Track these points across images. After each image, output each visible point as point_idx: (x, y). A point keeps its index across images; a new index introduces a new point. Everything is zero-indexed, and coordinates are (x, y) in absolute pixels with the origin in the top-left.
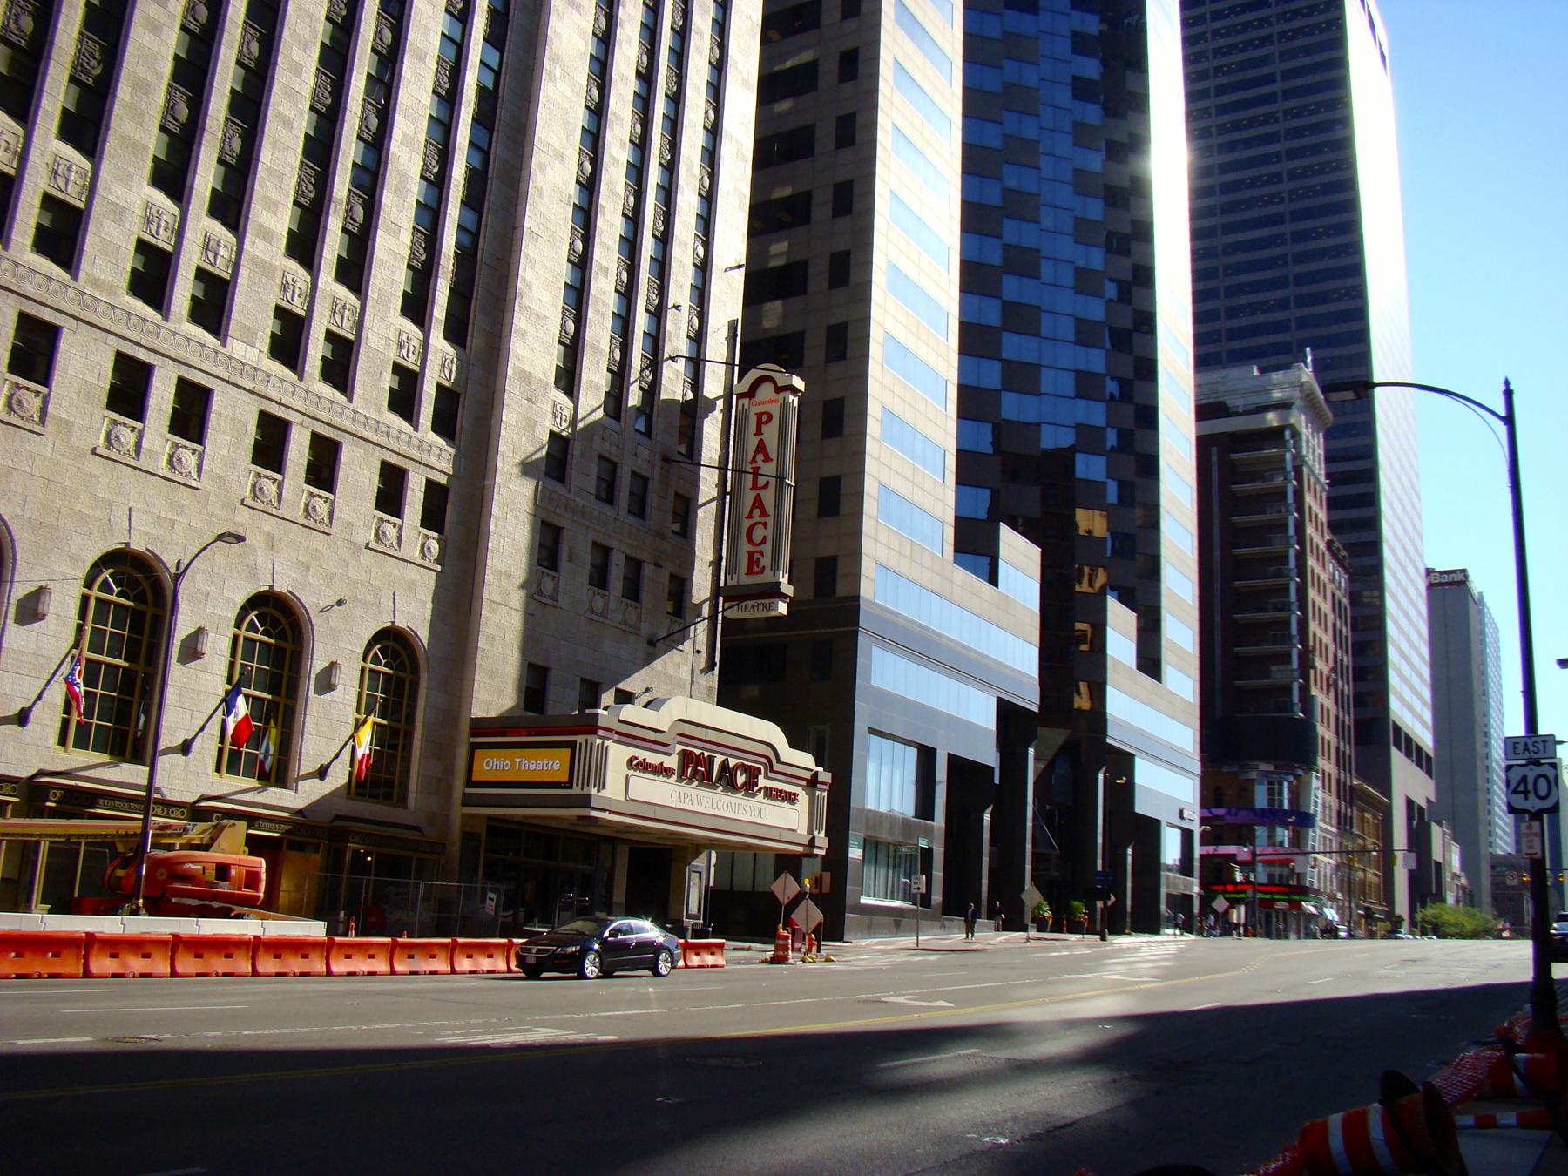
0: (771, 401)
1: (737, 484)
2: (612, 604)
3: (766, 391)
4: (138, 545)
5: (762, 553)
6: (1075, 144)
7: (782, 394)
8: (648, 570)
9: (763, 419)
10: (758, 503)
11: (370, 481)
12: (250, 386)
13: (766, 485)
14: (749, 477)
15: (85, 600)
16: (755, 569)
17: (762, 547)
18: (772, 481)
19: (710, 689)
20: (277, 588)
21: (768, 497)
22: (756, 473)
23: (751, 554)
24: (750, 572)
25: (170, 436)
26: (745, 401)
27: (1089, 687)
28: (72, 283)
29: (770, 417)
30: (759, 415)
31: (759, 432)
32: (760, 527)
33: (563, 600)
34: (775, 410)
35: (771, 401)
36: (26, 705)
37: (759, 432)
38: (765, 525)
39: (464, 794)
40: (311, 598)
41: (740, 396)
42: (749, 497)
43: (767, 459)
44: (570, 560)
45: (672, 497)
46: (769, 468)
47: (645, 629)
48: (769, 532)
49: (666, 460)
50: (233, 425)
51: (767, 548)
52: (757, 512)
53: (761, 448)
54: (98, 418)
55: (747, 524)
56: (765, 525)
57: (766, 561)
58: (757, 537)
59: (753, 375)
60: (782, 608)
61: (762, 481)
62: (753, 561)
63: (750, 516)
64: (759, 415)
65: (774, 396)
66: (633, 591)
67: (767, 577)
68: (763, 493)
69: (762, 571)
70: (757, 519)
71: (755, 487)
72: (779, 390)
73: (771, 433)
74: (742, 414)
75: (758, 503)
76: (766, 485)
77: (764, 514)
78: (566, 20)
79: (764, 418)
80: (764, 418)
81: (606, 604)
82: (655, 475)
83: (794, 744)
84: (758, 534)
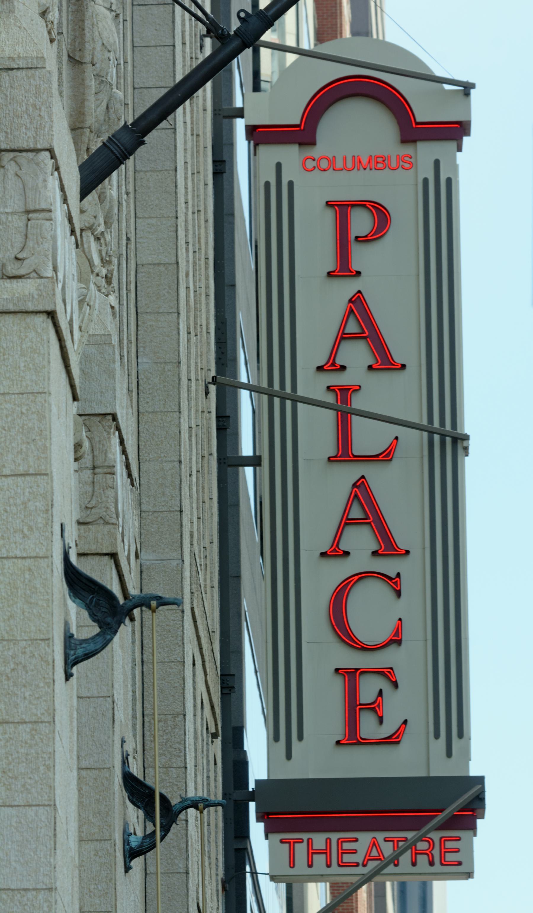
1: (280, 433)
6: (225, 172)
10: (363, 508)
16: (368, 726)
18: (412, 441)
24: (352, 738)
26: (289, 155)
27: (218, 390)
30: (342, 209)
31: (343, 269)
38: (394, 582)
41: (257, 135)
42: (323, 495)
43: (384, 362)
46: (379, 393)
48: (413, 608)
51: (410, 662)
52: (361, 541)
53: (360, 321)
55: (318, 582)
56: (394, 582)
61: (367, 437)
63: (335, 552)
68: (379, 478)
74: (277, 197)
75: (363, 508)
77: (387, 546)
78: (27, 293)
80: (361, 223)
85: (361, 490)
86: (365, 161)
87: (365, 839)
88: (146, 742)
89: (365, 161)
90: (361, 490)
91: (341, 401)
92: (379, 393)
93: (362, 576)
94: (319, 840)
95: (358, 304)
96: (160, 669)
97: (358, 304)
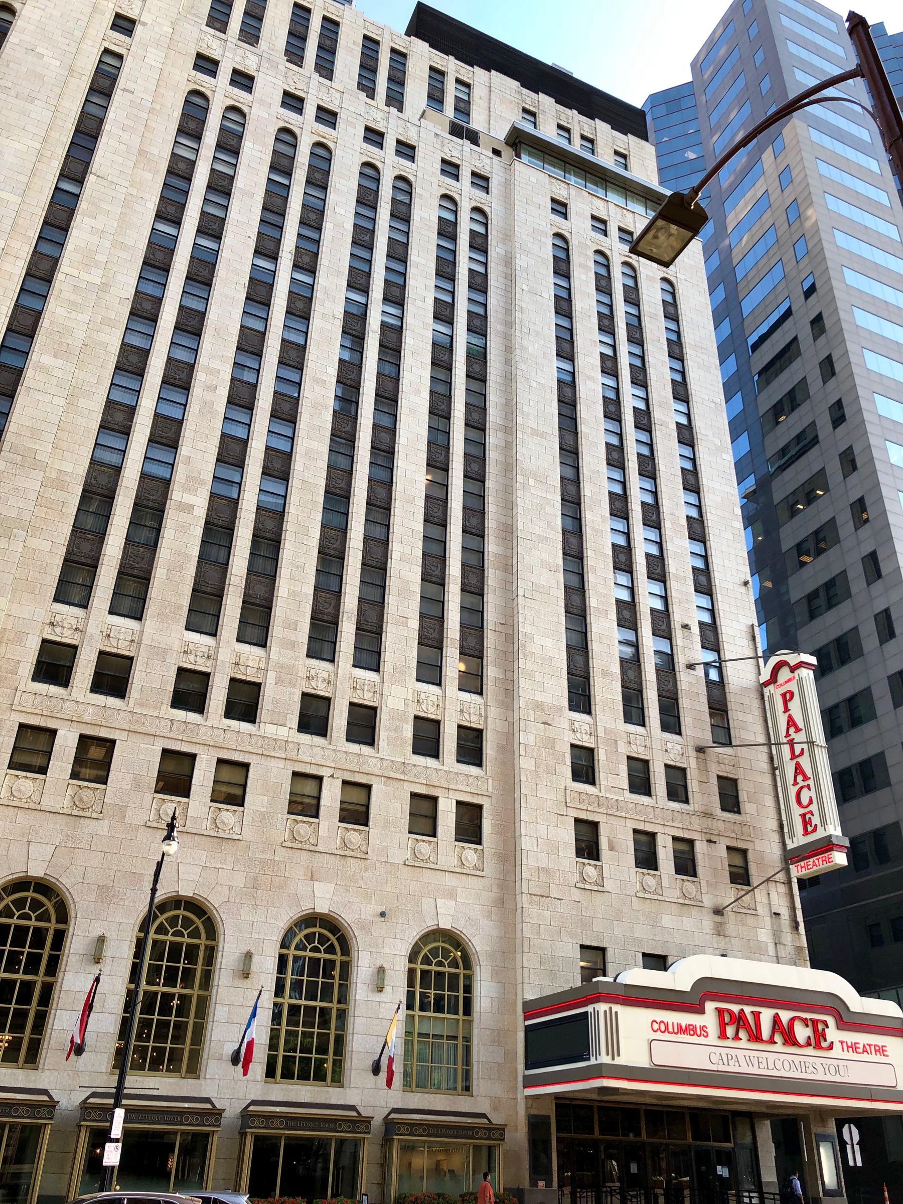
0: (790, 680)
2: (665, 882)
3: (784, 674)
4: (445, 924)
5: (811, 813)
7: (796, 672)
8: (700, 848)
9: (787, 697)
10: (798, 769)
11: (401, 809)
12: (469, 790)
13: (802, 753)
14: (786, 749)
15: (411, 972)
16: (810, 829)
17: (811, 808)
18: (805, 746)
19: (799, 949)
20: (442, 926)
21: (805, 762)
22: (791, 743)
23: (803, 816)
24: (806, 833)
25: (578, 859)
28: (442, 767)
29: (792, 695)
31: (786, 709)
32: (805, 790)
33: (608, 885)
34: (793, 687)
35: (790, 680)
36: (376, 1058)
37: (786, 709)
38: (808, 787)
39: (524, 1077)
40: (353, 914)
43: (798, 730)
44: (612, 849)
45: (715, 781)
46: (800, 737)
47: (708, 901)
48: (812, 793)
49: (700, 750)
50: (390, 807)
52: (800, 778)
53: (791, 722)
54: (633, 874)
55: (793, 791)
56: (808, 787)
57: (816, 820)
58: (805, 801)
59: (773, 661)
60: (840, 859)
62: (806, 823)
64: (784, 695)
65: (790, 675)
66: (686, 865)
67: (820, 834)
69: (815, 830)
70: (801, 784)
71: (793, 756)
72: (793, 669)
73: (795, 706)
75: (798, 769)
76: (802, 753)
77: (806, 778)
79: (788, 696)
80: (788, 696)
81: (660, 883)
82: (691, 764)
83: (864, 990)
84: (805, 797)
85: (798, 764)
86: (684, 1027)
87: (811, 860)
88: (759, 721)
89: (684, 1027)
90: (798, 764)
91: (549, 1124)
92: (800, 737)
93: (802, 788)
94: (802, 863)
95: (790, 717)
96: (416, 1200)
97: (790, 717)
